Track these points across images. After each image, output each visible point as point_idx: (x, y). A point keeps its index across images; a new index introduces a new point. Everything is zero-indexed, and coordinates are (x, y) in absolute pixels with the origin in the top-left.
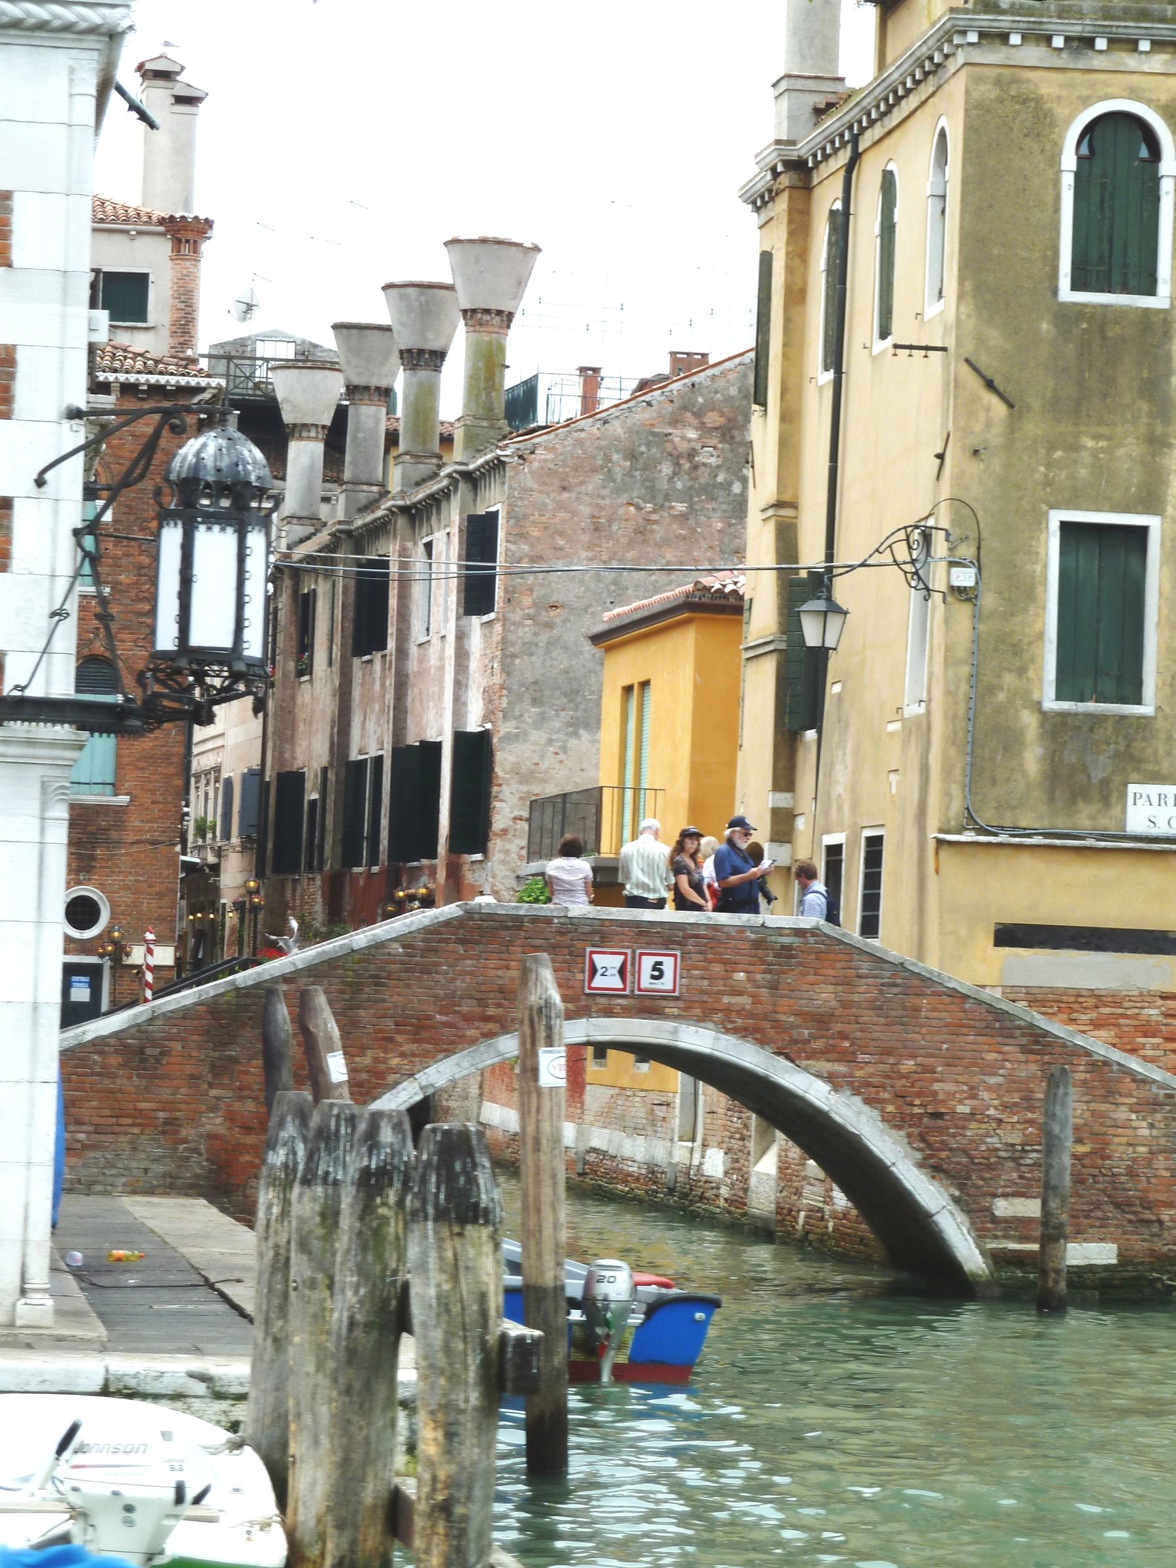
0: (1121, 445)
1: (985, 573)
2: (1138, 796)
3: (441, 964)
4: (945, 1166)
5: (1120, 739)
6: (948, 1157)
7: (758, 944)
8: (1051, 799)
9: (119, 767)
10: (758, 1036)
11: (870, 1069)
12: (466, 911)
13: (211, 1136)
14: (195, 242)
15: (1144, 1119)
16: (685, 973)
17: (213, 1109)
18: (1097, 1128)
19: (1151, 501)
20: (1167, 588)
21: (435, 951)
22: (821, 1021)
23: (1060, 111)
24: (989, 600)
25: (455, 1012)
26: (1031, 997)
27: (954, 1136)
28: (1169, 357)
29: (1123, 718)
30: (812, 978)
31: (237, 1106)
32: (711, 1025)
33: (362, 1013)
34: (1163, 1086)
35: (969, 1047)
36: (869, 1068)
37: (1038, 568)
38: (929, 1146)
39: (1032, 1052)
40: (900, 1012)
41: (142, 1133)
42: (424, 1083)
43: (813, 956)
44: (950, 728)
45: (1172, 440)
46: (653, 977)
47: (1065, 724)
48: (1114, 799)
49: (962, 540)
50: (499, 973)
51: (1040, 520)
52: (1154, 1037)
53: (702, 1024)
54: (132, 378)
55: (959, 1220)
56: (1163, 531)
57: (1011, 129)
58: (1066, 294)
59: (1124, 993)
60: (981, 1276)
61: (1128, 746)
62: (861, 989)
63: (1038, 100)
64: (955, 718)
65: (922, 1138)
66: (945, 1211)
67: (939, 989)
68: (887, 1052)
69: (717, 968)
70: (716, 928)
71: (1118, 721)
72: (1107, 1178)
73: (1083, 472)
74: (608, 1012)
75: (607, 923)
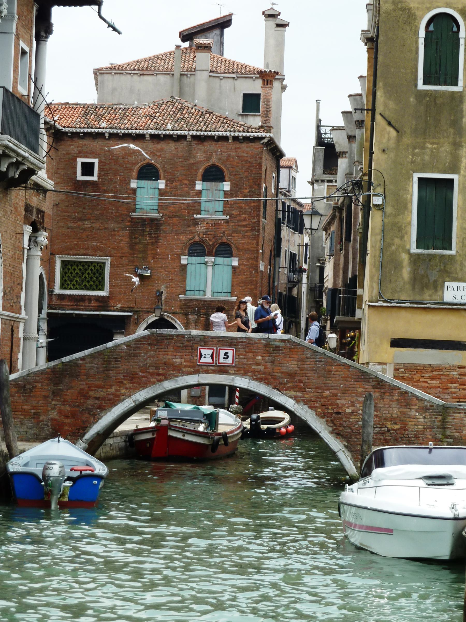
0: (442, 146)
1: (387, 199)
2: (449, 287)
3: (141, 353)
4: (341, 433)
5: (442, 264)
6: (343, 430)
7: (266, 345)
8: (414, 288)
9: (233, 286)
10: (266, 381)
11: (311, 395)
12: (151, 333)
13: (52, 420)
14: (270, 81)
15: (421, 415)
16: (237, 357)
17: (53, 409)
18: (402, 418)
19: (454, 169)
20: (461, 203)
21: (139, 348)
22: (292, 375)
23: (418, 13)
24: (389, 209)
25: (147, 372)
26: (406, 368)
27: (345, 421)
28: (462, 111)
29: (443, 256)
30: (288, 358)
31: (62, 408)
32: (247, 377)
33: (111, 372)
34: (429, 402)
35: (351, 386)
36: (311, 394)
37: (409, 196)
38: (335, 425)
39: (377, 388)
40: (323, 372)
41: (25, 418)
42: (134, 399)
43: (289, 350)
44: (373, 260)
45: (463, 144)
46: (224, 358)
47: (419, 258)
48: (439, 288)
49: (378, 186)
50: (164, 357)
51: (410, 177)
52: (455, 383)
53: (244, 377)
54: (236, 134)
55: (347, 455)
56: (459, 181)
57: (398, 21)
58: (421, 86)
59: (443, 366)
60: (355, 477)
61: (445, 267)
62: (308, 363)
63: (409, 9)
64: (375, 256)
65: (332, 422)
66: (341, 451)
67: (339, 363)
68: (318, 388)
69: (250, 355)
70: (250, 339)
71: (441, 257)
72: (407, 439)
73: (427, 158)
74: (207, 372)
75: (206, 337)
